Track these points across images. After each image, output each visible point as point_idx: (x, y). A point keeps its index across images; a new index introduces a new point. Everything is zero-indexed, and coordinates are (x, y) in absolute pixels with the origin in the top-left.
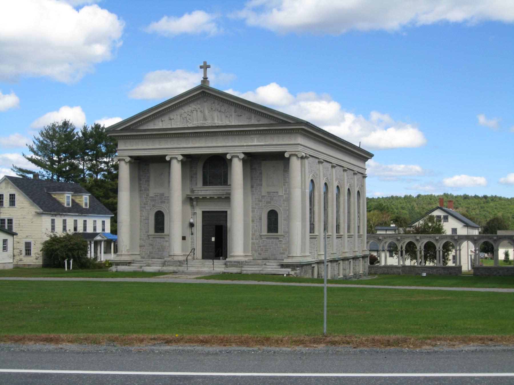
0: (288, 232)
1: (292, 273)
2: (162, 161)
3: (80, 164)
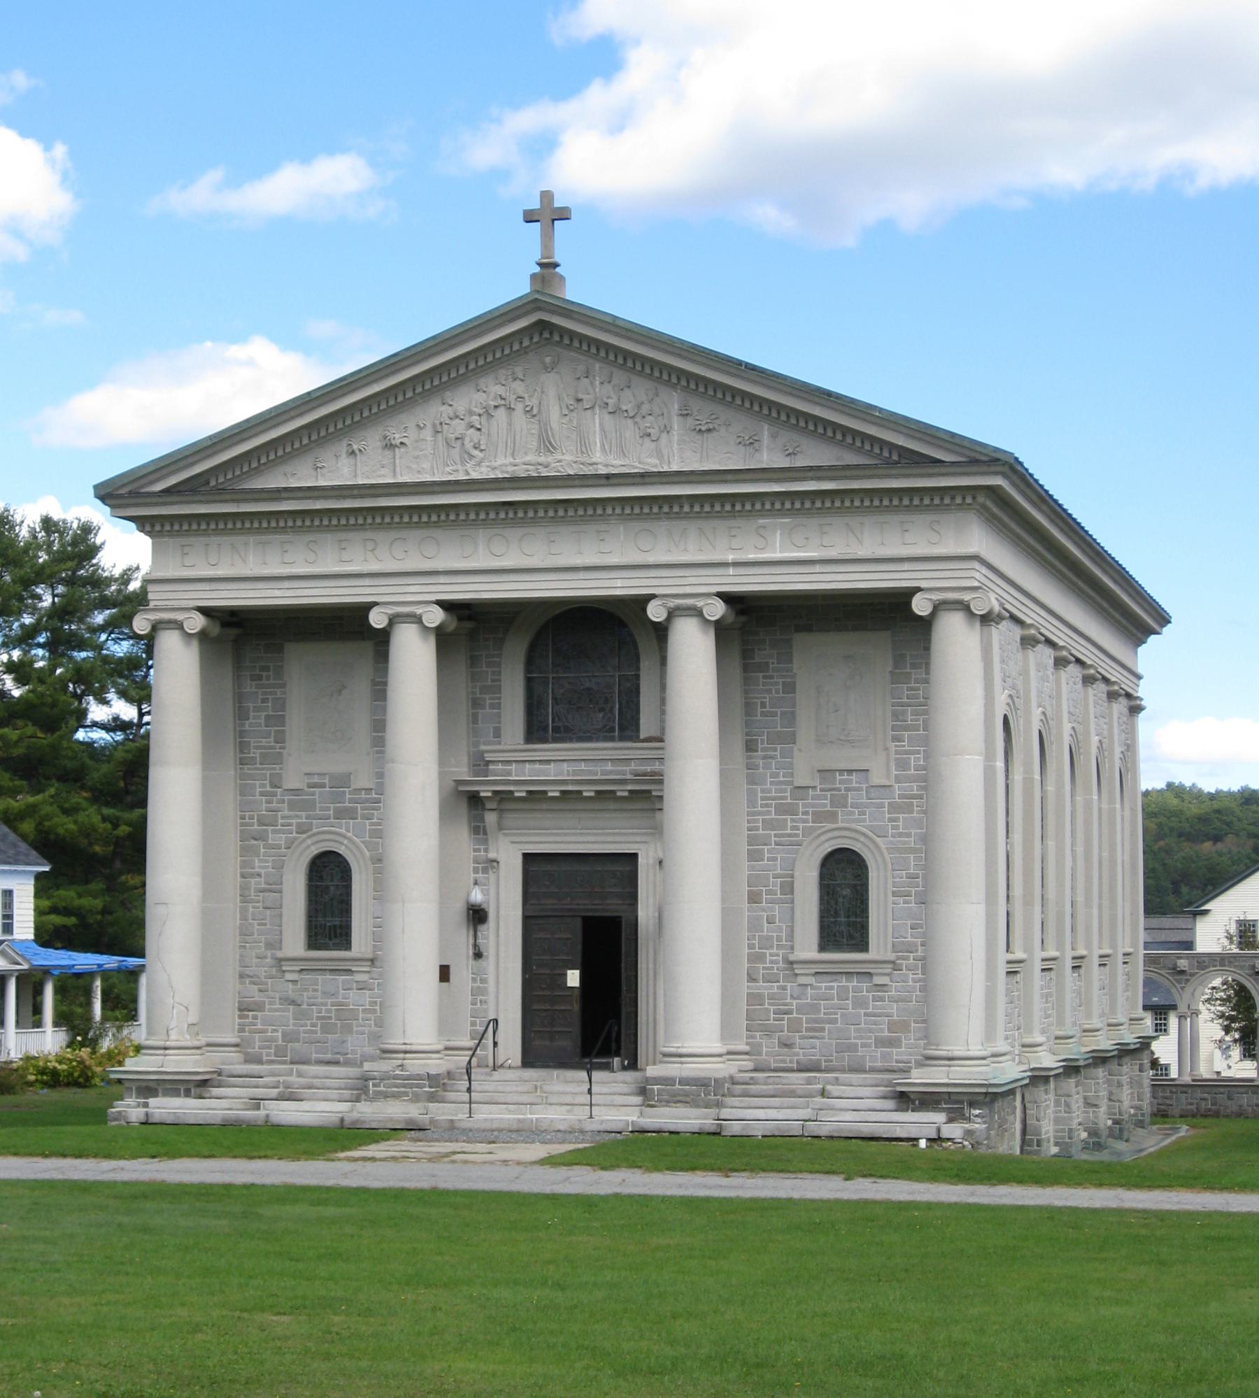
0: (923, 955)
1: (954, 1131)
2: (347, 631)
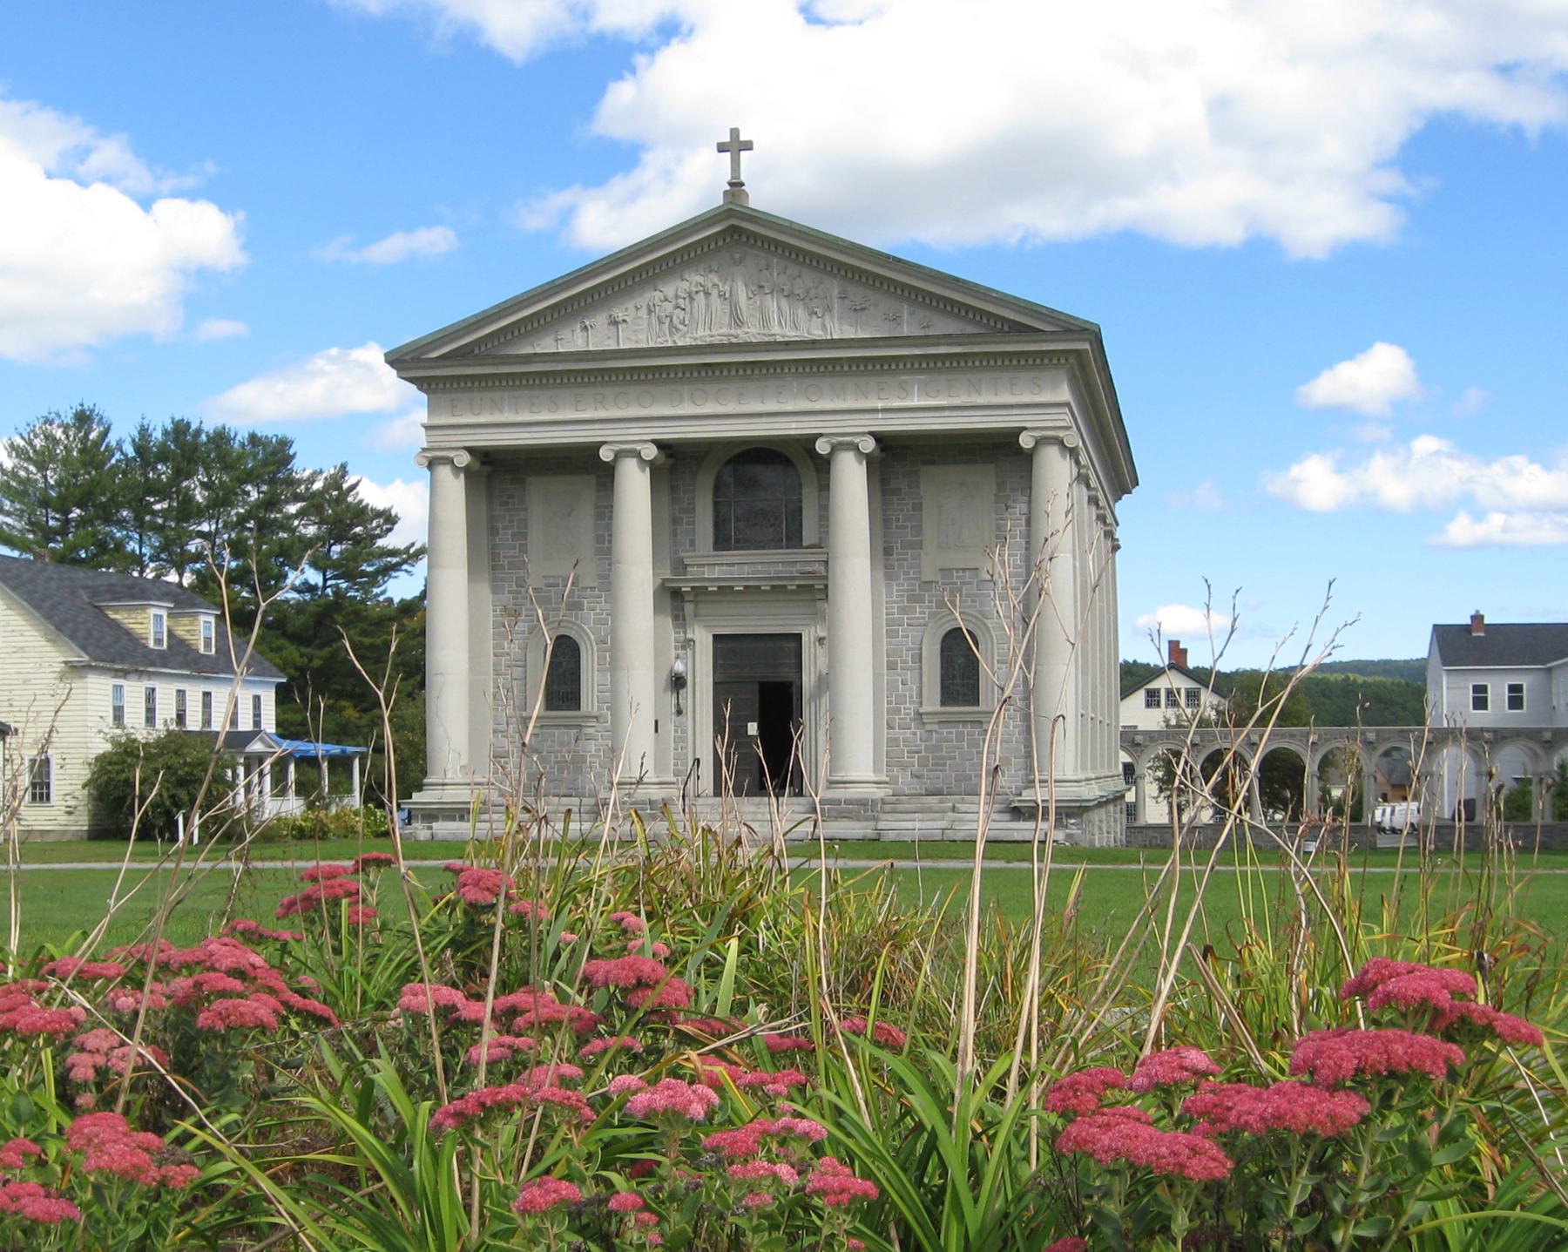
2: (586, 468)
3: (131, 538)
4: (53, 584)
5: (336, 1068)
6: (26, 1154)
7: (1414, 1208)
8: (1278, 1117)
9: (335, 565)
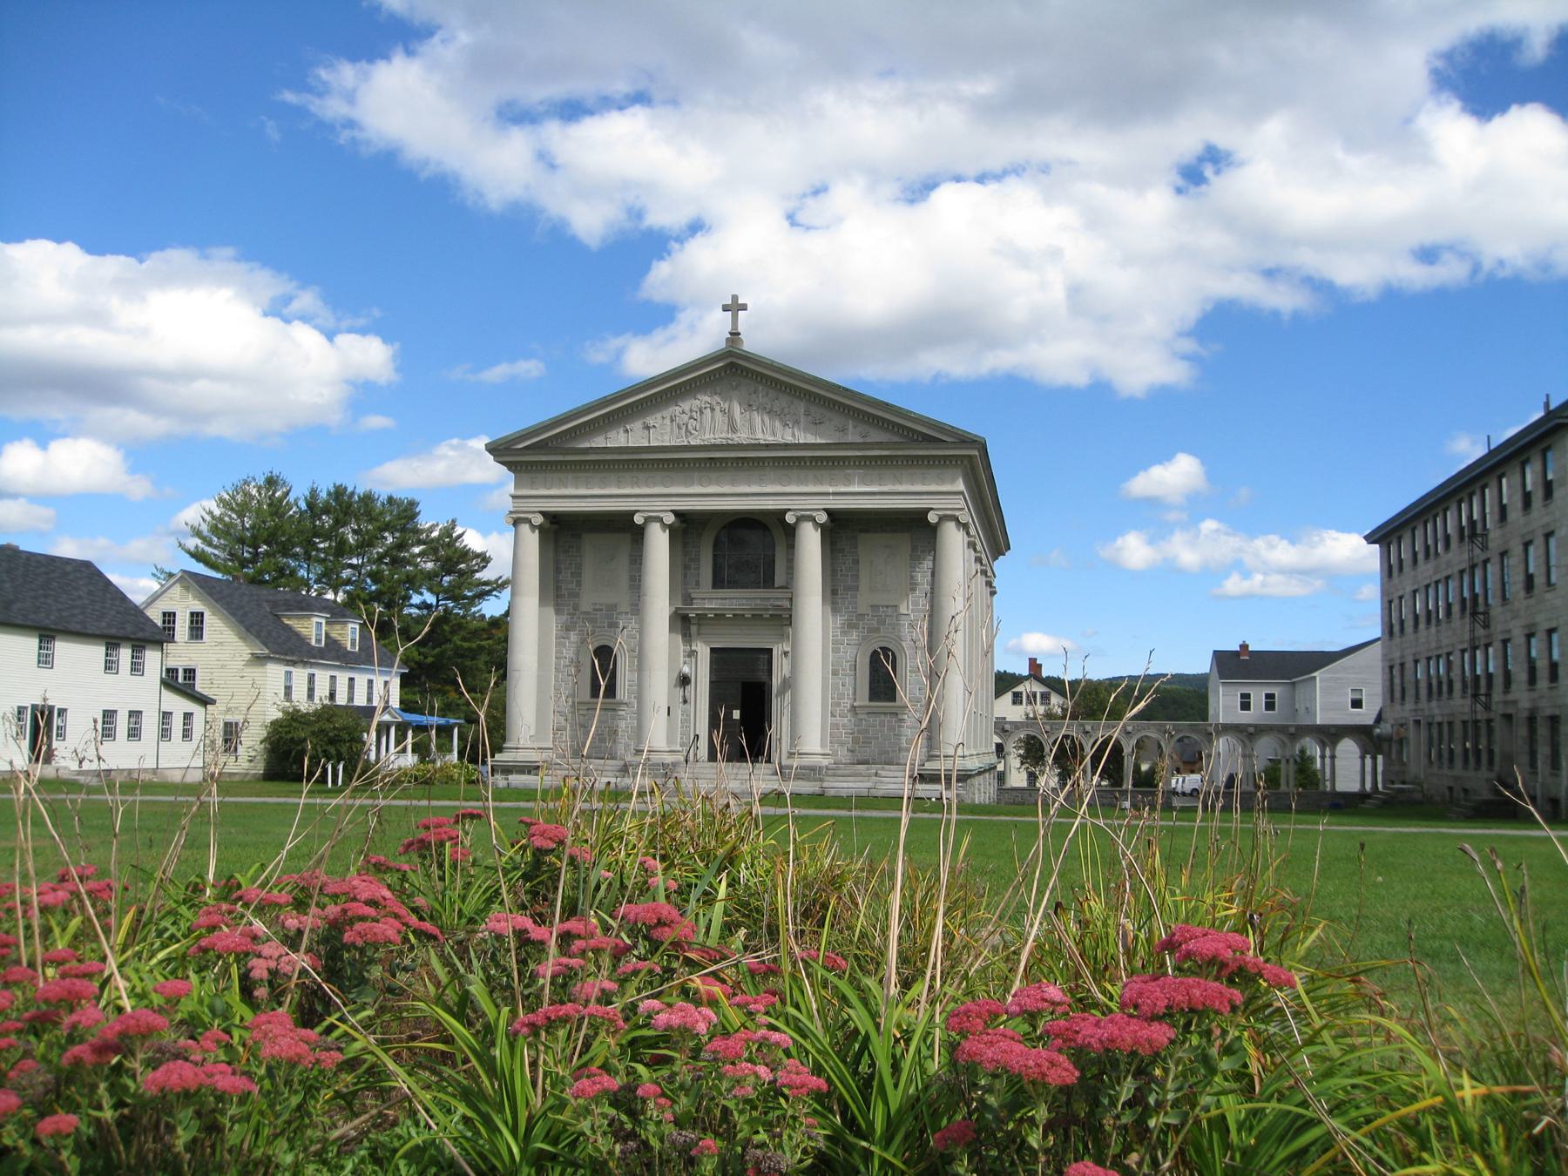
2: (624, 530)
4: (246, 599)
5: (442, 973)
6: (218, 1042)
7: (1205, 1100)
8: (1112, 1041)
9: (446, 591)
